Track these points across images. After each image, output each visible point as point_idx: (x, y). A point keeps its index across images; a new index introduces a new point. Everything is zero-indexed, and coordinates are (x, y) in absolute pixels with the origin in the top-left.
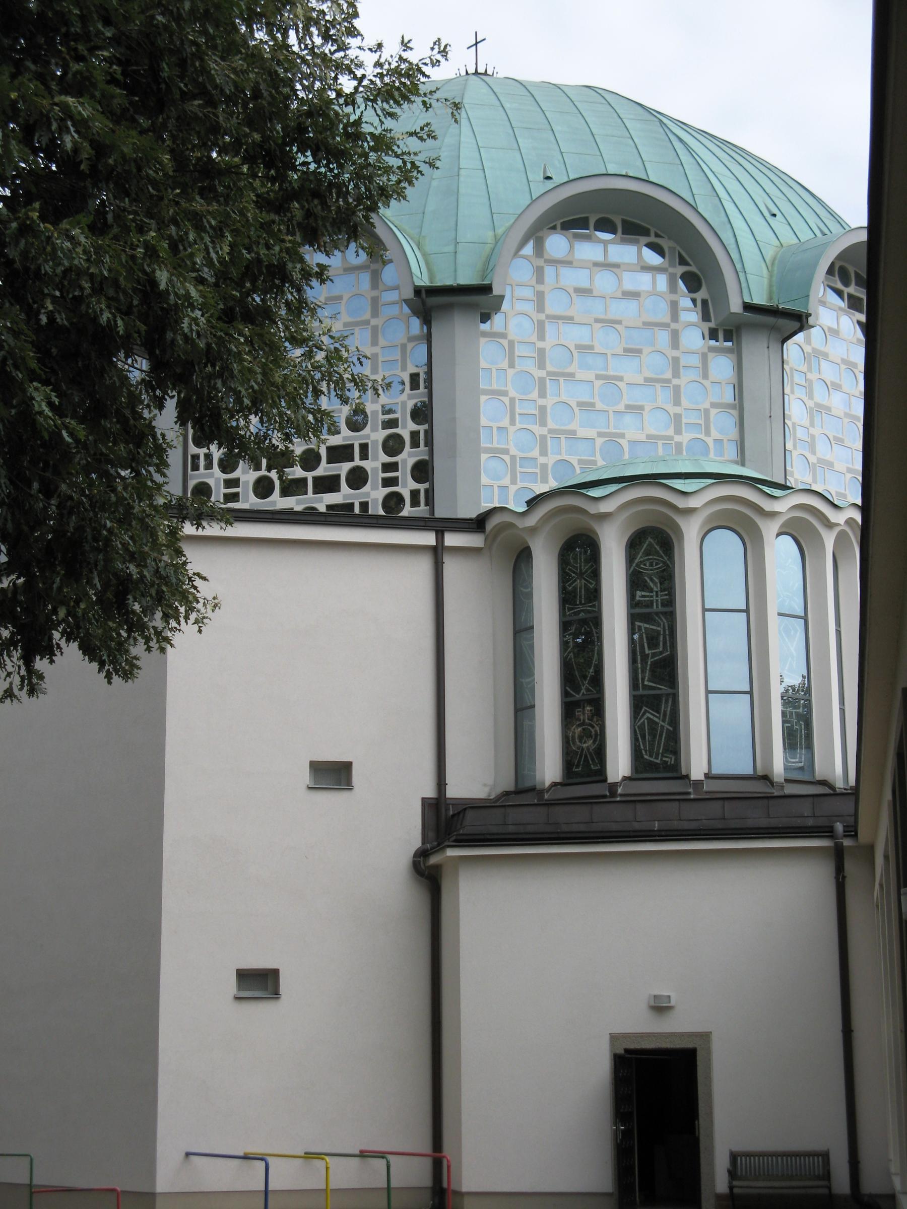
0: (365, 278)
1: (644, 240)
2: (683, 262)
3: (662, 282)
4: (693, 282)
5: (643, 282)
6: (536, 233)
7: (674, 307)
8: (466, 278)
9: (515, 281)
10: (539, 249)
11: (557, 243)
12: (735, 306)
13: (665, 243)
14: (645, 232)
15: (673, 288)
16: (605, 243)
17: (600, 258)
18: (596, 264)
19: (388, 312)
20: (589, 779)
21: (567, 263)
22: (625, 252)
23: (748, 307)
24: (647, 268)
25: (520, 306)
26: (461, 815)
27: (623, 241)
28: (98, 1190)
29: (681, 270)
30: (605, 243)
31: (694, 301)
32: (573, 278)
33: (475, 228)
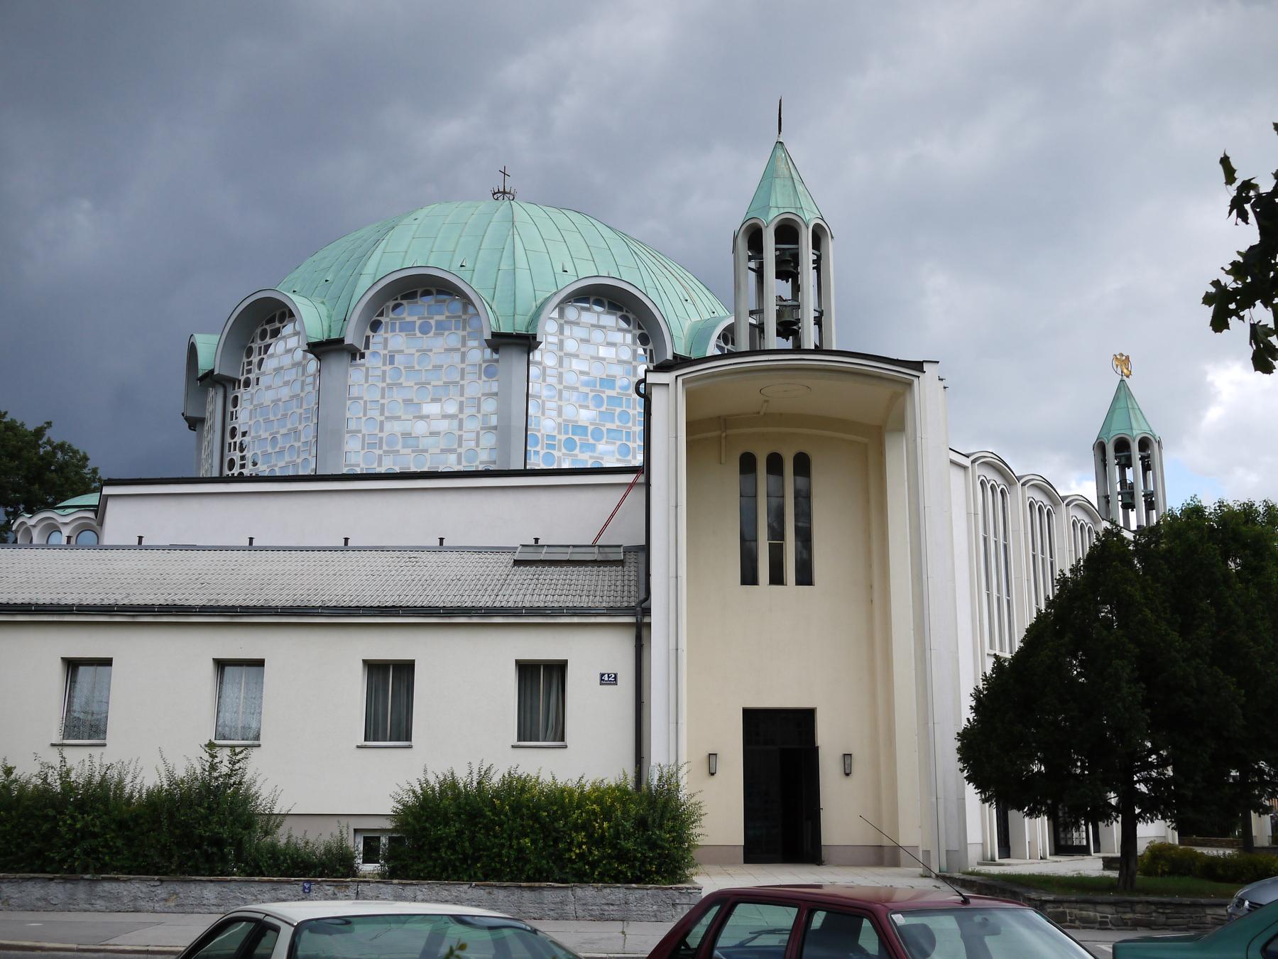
0: (456, 357)
1: (620, 313)
2: (640, 328)
3: (629, 337)
4: (644, 339)
5: (618, 337)
6: (562, 306)
7: (635, 352)
8: (521, 329)
9: (548, 331)
10: (562, 314)
11: (571, 312)
12: (669, 356)
13: (631, 317)
14: (621, 309)
15: (634, 343)
16: (599, 313)
17: (595, 322)
18: (593, 326)
19: (468, 377)
20: (576, 620)
21: (577, 324)
22: (610, 320)
23: (675, 356)
24: (620, 330)
25: (550, 347)
26: (782, 166)
27: (608, 313)
28: (371, 549)
29: (638, 332)
30: (599, 313)
31: (645, 350)
32: (580, 332)
33: (526, 304)
